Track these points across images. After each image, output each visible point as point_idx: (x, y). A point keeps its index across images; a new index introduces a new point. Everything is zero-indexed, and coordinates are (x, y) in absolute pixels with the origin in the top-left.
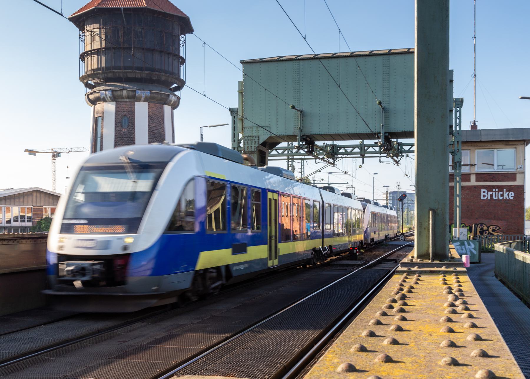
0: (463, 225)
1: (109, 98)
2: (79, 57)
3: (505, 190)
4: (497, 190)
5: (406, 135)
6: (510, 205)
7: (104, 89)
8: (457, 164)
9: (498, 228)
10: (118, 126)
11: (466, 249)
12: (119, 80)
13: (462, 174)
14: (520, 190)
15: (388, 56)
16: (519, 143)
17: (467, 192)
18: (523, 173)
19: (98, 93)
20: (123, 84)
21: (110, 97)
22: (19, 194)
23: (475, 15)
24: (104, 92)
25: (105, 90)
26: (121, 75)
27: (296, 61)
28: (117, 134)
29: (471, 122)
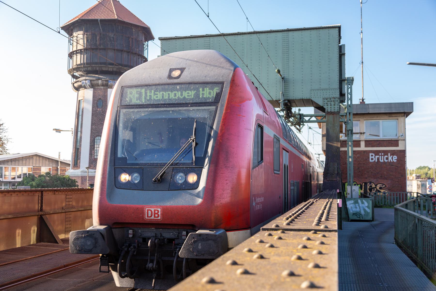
0: (355, 183)
1: (88, 86)
2: (67, 56)
3: (389, 154)
4: (383, 154)
5: (305, 105)
6: (394, 167)
7: (85, 79)
8: (350, 132)
9: (384, 186)
10: (94, 107)
11: (359, 207)
12: (96, 72)
13: (354, 141)
14: (402, 155)
15: (288, 32)
16: (401, 115)
17: (358, 156)
18: (405, 140)
19: (81, 82)
20: (99, 75)
21: (89, 85)
22: (22, 157)
23: (361, 10)
24: (84, 81)
25: (86, 80)
26: (98, 69)
27: (207, 38)
28: (93, 113)
29: (360, 99)
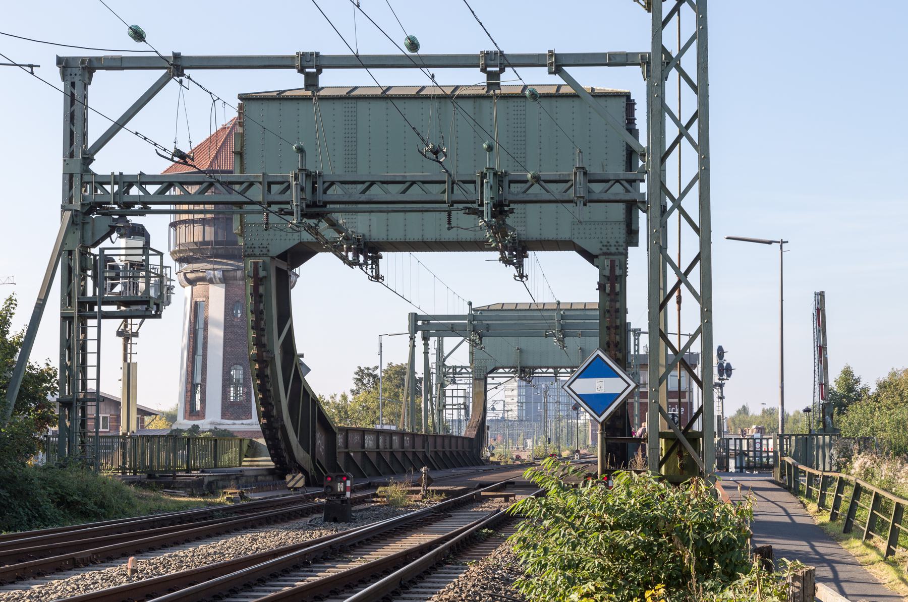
1: (218, 280)
21: (219, 278)
24: (212, 272)
25: (214, 270)
